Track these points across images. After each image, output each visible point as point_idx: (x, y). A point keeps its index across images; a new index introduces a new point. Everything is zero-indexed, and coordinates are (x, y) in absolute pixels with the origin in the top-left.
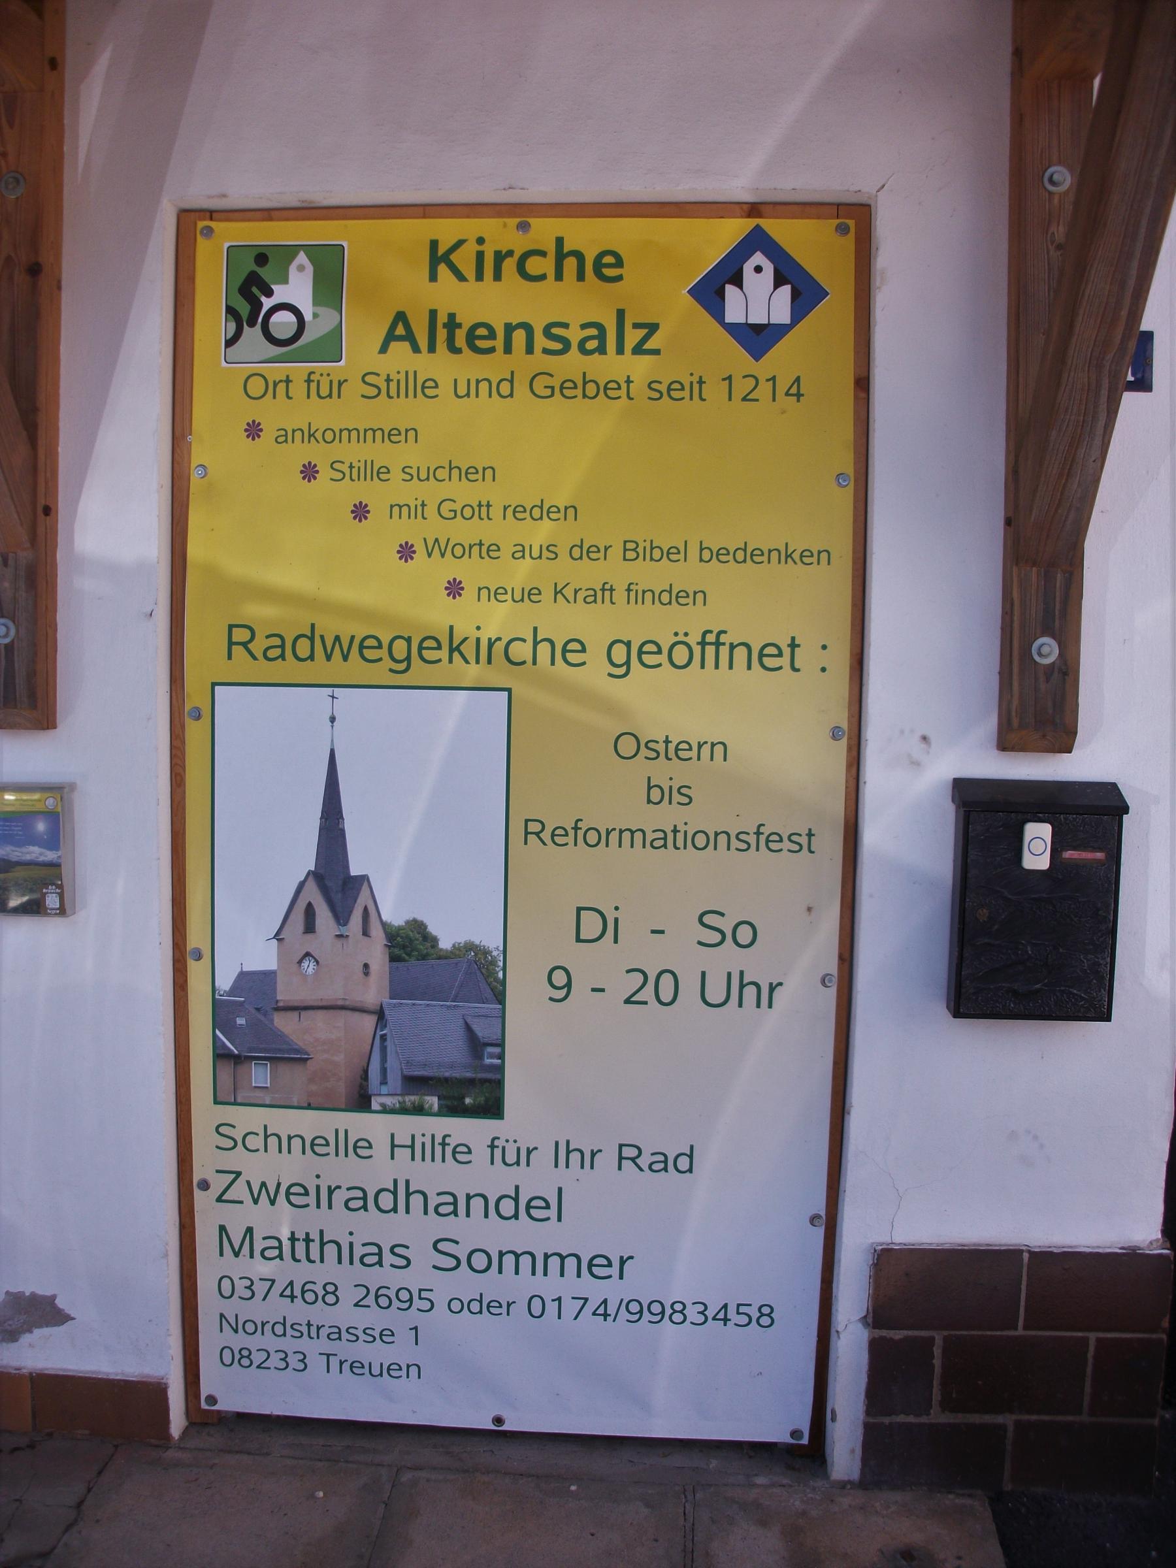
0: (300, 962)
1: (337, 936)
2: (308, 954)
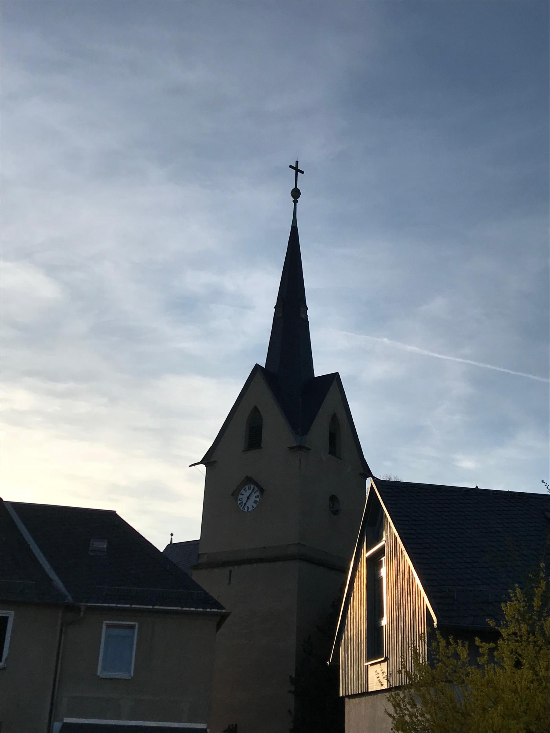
0: (236, 493)
1: (291, 448)
2: (249, 480)
